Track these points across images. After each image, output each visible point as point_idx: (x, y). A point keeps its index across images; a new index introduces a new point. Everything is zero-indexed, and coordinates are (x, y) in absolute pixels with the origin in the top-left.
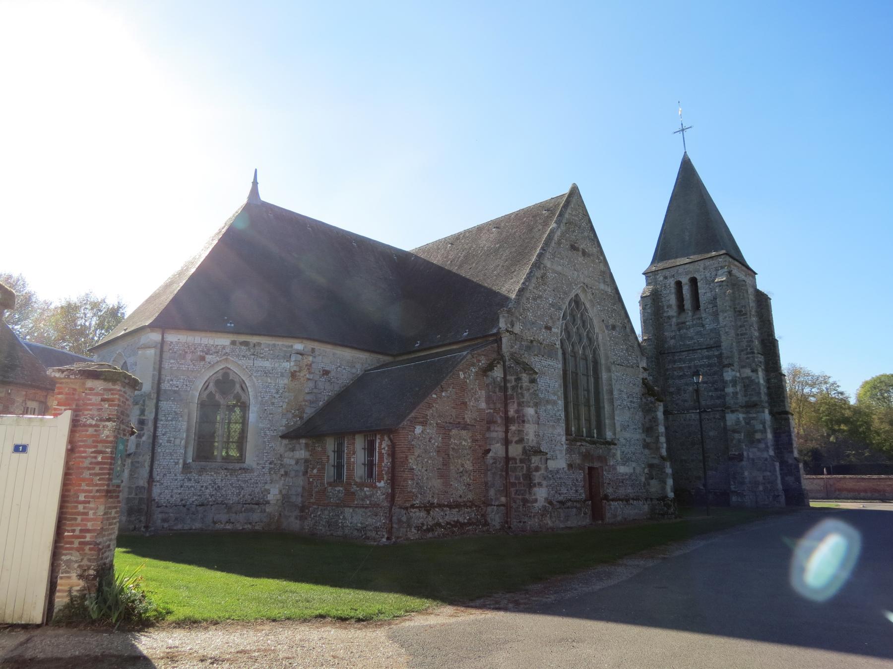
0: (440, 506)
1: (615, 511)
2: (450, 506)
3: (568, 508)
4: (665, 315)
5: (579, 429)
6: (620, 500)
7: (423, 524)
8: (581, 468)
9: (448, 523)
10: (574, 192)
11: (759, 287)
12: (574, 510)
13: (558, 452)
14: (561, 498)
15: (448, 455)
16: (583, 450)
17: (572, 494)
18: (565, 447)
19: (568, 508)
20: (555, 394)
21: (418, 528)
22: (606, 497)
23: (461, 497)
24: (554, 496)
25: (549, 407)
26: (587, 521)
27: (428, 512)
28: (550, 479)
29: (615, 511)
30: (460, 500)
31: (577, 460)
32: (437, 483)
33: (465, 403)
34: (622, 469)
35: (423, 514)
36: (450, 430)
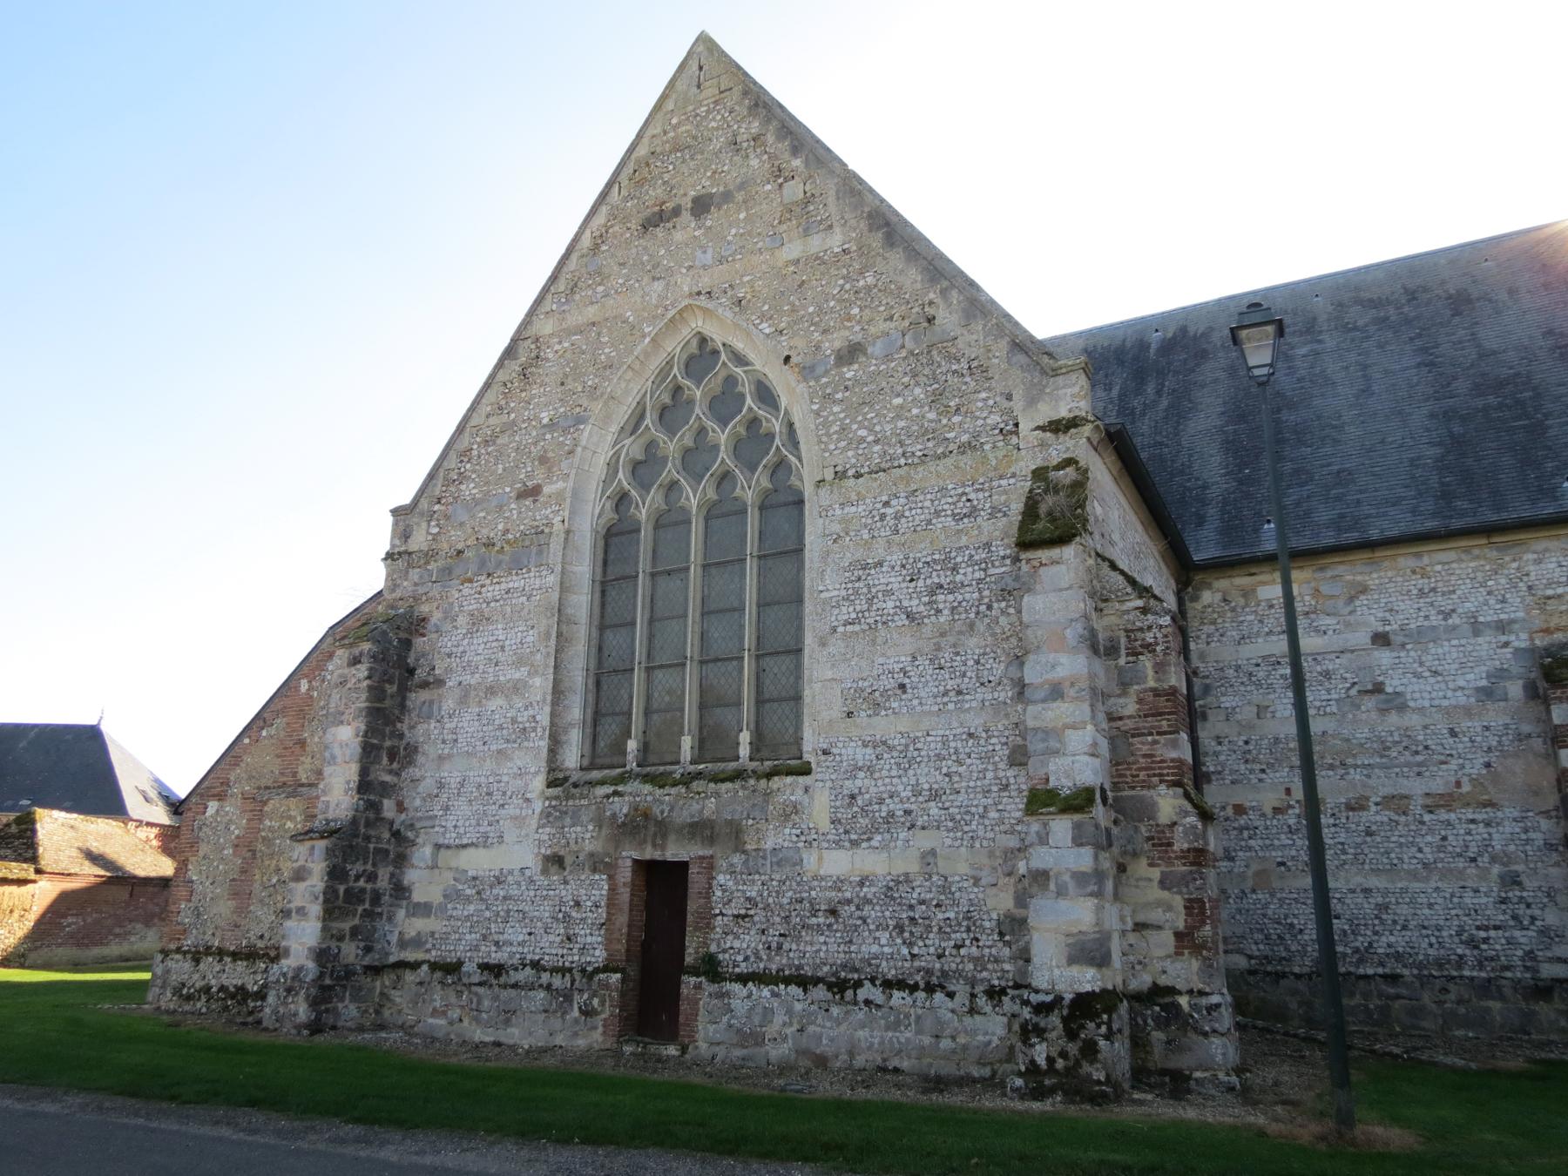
0: (221, 953)
1: (729, 1025)
2: (235, 956)
3: (515, 986)
4: (399, 725)
5: (662, 718)
6: (804, 982)
7: (184, 985)
8: (597, 864)
9: (222, 988)
10: (705, 44)
11: (1047, 318)
12: (542, 994)
13: (506, 825)
14: (496, 957)
15: (254, 852)
16: (621, 807)
17: (549, 947)
18: (538, 806)
19: (515, 986)
20: (519, 662)
21: (177, 991)
22: (711, 969)
23: (262, 937)
24: (476, 948)
25: (496, 703)
26: (595, 1037)
27: (197, 961)
28: (468, 900)
29: (729, 1025)
30: (260, 944)
31: (586, 838)
32: (224, 909)
33: (302, 743)
34: (836, 863)
35: (188, 965)
36: (265, 803)
